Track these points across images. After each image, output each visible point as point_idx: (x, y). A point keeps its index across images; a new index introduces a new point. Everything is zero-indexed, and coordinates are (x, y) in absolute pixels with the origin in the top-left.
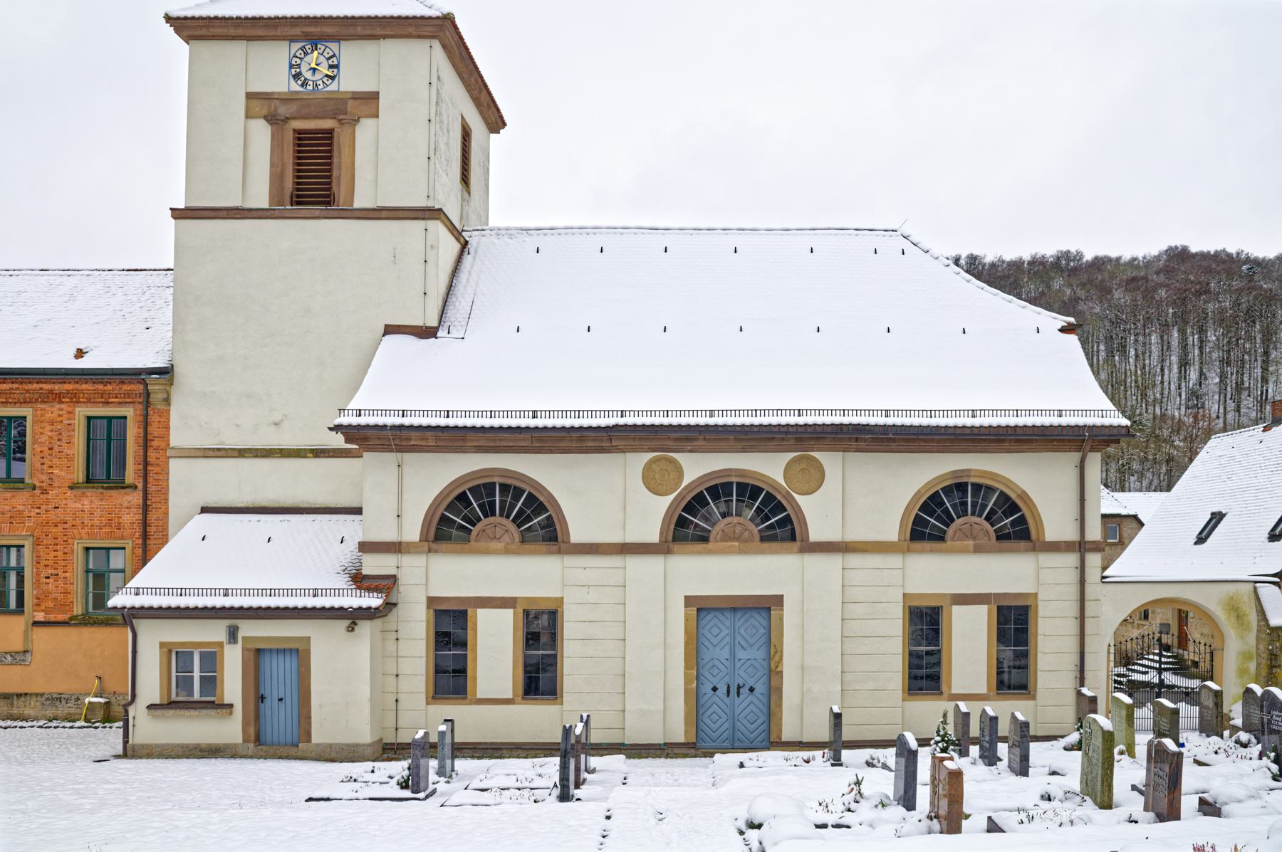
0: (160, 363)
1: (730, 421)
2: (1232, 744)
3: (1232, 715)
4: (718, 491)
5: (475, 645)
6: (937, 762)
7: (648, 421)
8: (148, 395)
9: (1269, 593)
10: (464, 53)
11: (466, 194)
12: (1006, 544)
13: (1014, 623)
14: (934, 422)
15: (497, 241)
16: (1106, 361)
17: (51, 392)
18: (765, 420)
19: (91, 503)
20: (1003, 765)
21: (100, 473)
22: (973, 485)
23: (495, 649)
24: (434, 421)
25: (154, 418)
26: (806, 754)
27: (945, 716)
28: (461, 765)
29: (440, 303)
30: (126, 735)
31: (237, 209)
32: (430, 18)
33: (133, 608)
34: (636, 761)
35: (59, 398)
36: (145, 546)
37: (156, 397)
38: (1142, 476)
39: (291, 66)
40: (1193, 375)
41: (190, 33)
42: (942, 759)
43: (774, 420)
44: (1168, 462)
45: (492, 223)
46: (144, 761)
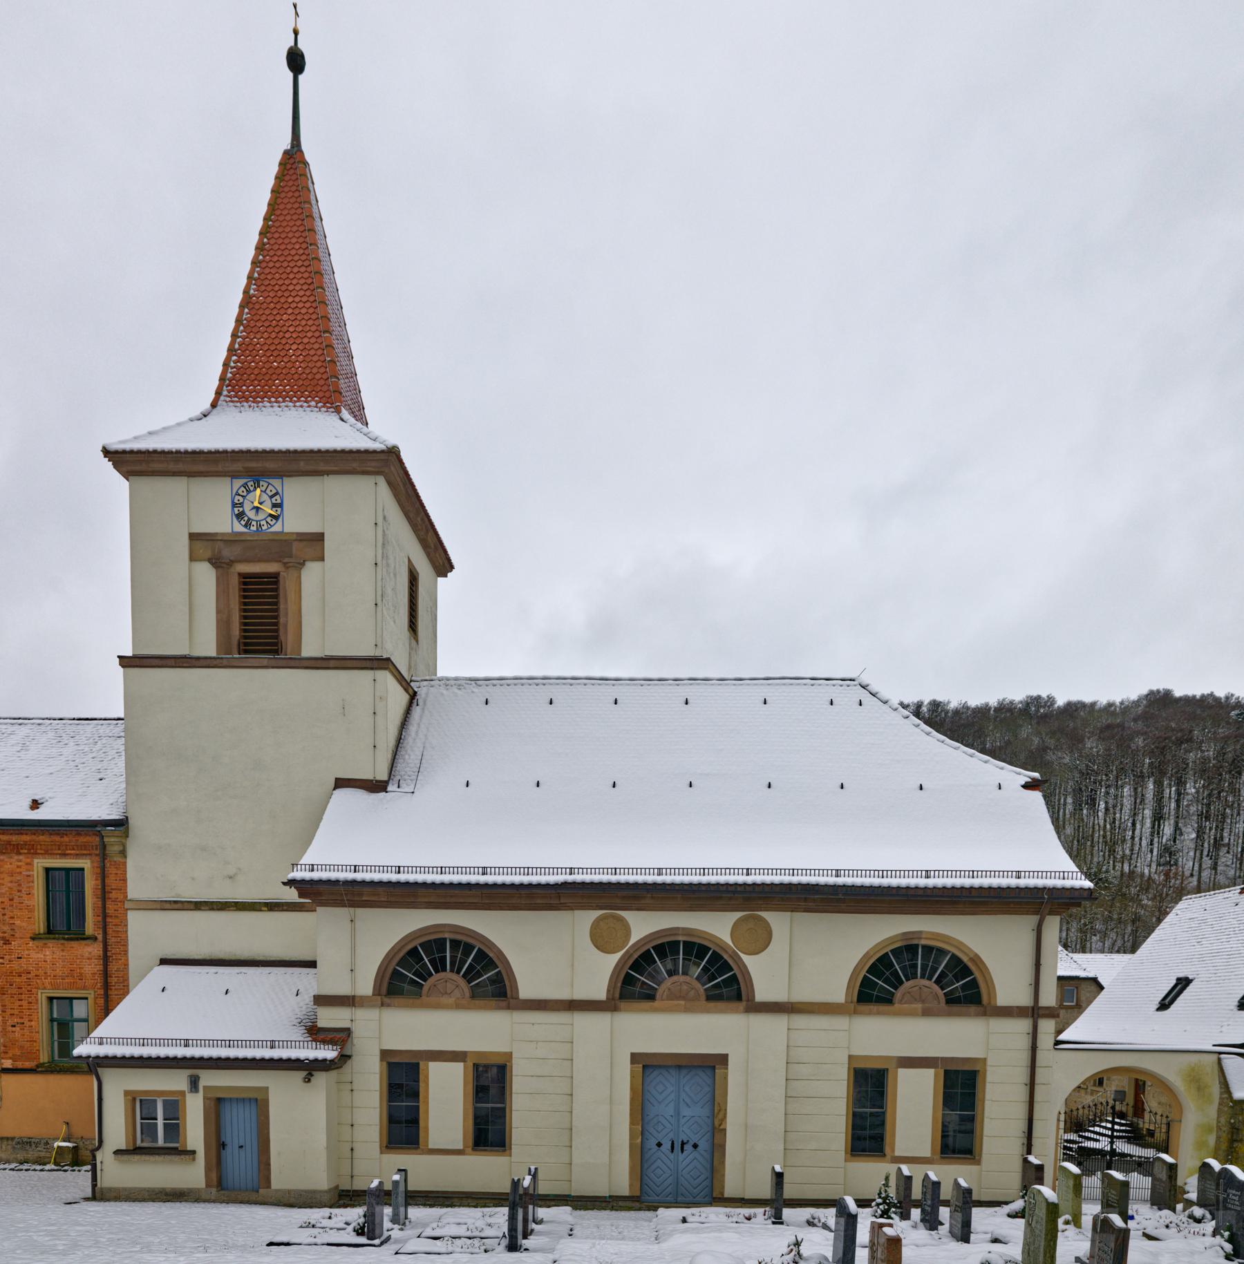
0: (115, 816)
1: (678, 879)
2: (1185, 1219)
3: (1187, 1188)
4: (666, 947)
5: (427, 1097)
6: (876, 1229)
7: (596, 878)
8: (104, 847)
9: (1232, 1065)
10: (410, 491)
11: (414, 642)
12: (955, 1008)
13: (961, 1086)
14: (885, 882)
15: (459, 692)
16: (1073, 814)
17: (9, 843)
18: (713, 879)
19: (52, 955)
20: (944, 1229)
21: (60, 925)
22: (924, 947)
23: (446, 1101)
24: (385, 877)
25: (111, 870)
26: (747, 1211)
27: (887, 1178)
28: (415, 1213)
29: (390, 756)
30: (94, 1178)
31: (185, 657)
32: (375, 452)
33: (98, 1057)
34: (583, 1212)
35: (17, 849)
36: (106, 996)
37: (113, 849)
38: (1104, 935)
39: (234, 505)
40: (1168, 830)
41: (130, 468)
42: (881, 1226)
43: (722, 879)
44: (1133, 922)
45: (440, 674)
46: (112, 1203)
